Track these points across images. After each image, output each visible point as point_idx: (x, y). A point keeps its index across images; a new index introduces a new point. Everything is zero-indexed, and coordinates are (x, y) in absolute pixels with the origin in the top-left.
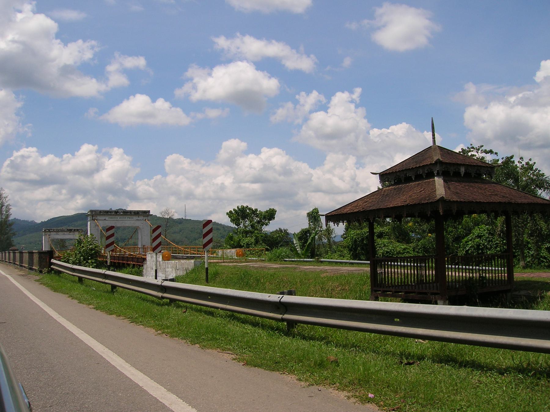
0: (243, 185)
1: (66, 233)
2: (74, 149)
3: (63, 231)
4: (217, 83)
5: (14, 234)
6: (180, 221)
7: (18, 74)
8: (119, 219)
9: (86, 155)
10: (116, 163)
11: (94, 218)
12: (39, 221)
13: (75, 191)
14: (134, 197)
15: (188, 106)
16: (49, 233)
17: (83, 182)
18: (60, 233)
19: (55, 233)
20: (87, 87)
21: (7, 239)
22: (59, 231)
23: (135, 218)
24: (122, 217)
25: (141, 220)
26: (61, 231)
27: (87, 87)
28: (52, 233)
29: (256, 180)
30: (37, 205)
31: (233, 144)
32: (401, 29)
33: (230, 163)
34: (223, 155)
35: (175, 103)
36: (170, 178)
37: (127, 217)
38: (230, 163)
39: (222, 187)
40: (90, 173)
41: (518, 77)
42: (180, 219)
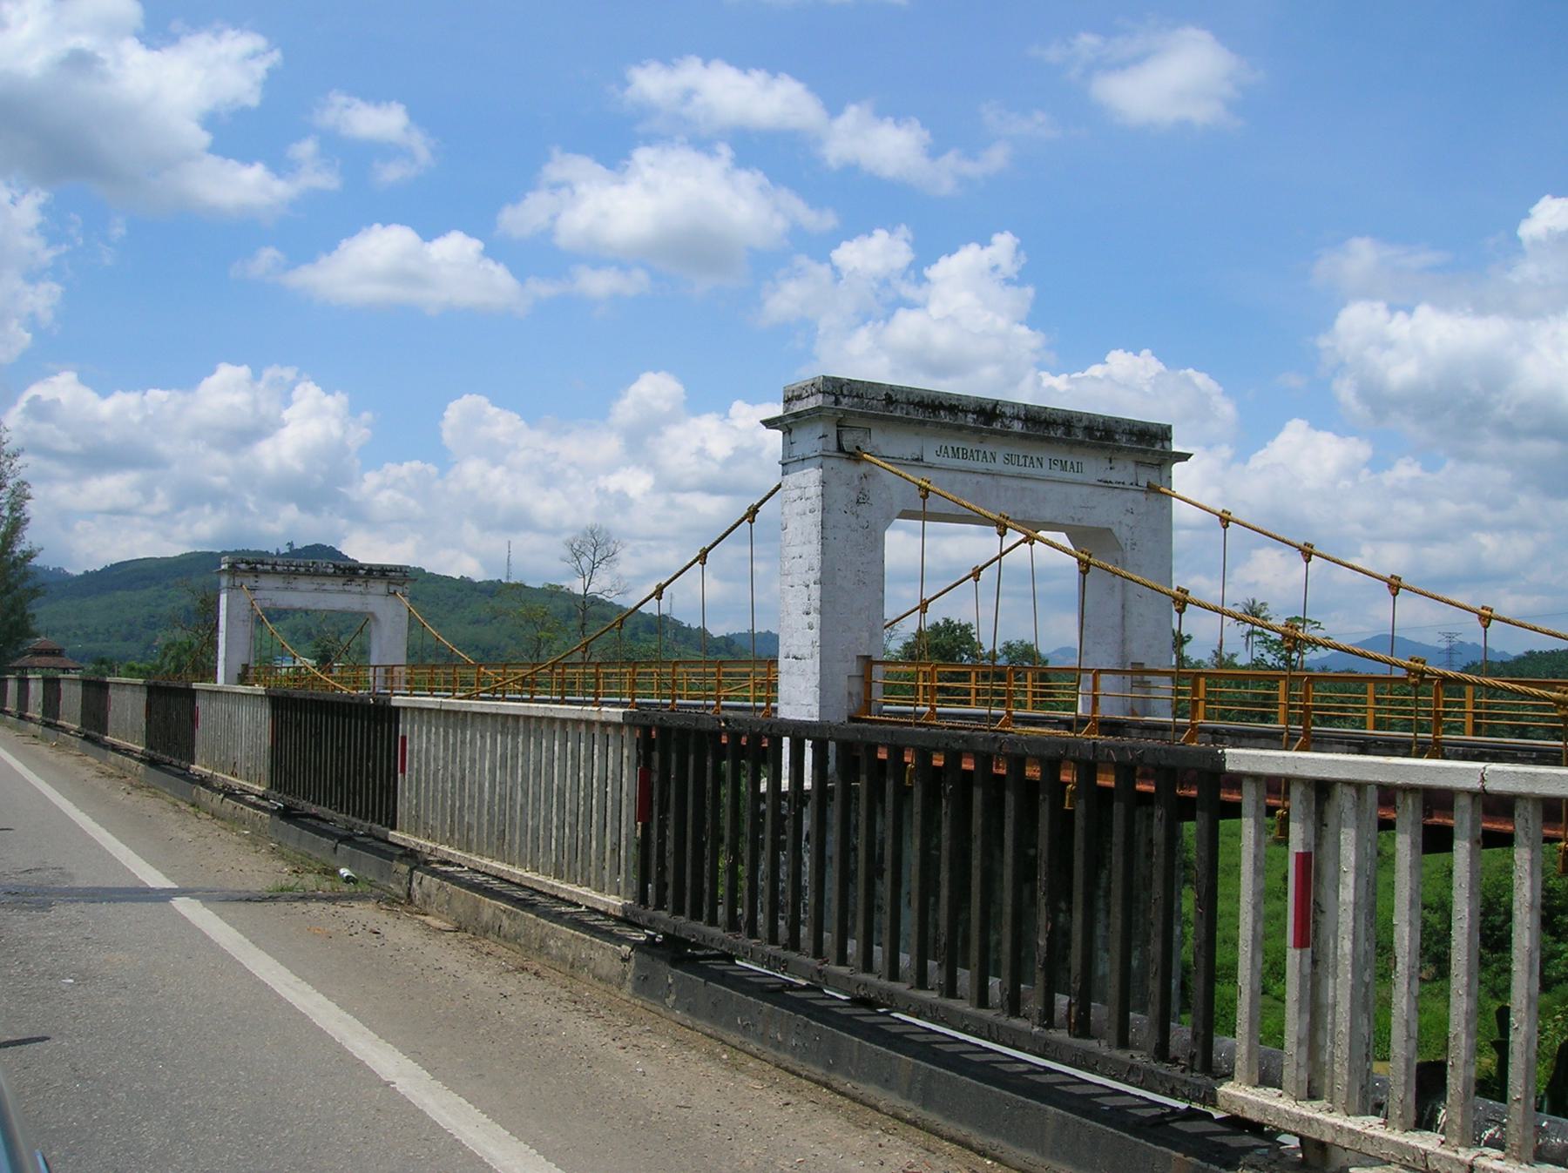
0: (681, 498)
1: (329, 584)
2: (188, 378)
3: (316, 574)
4: (622, 205)
5: (34, 592)
6: (492, 590)
7: (37, 135)
8: (998, 465)
9: (225, 390)
10: (309, 422)
11: (849, 440)
12: (77, 571)
13: (192, 496)
14: (359, 516)
15: (536, 257)
16: (250, 581)
17: (217, 467)
18: (303, 583)
19: (278, 582)
20: (244, 185)
21: (13, 610)
22: (296, 573)
23: (1094, 467)
24: (1018, 450)
25: (1120, 487)
26: (308, 573)
27: (244, 185)
28: (266, 582)
29: (712, 488)
30: (87, 527)
31: (654, 389)
32: (1172, 80)
33: (639, 442)
34: (626, 409)
35: (493, 251)
36: (472, 470)
37: (1046, 454)
38: (639, 442)
39: (623, 502)
40: (244, 435)
41: (1466, 250)
42: (491, 582)
